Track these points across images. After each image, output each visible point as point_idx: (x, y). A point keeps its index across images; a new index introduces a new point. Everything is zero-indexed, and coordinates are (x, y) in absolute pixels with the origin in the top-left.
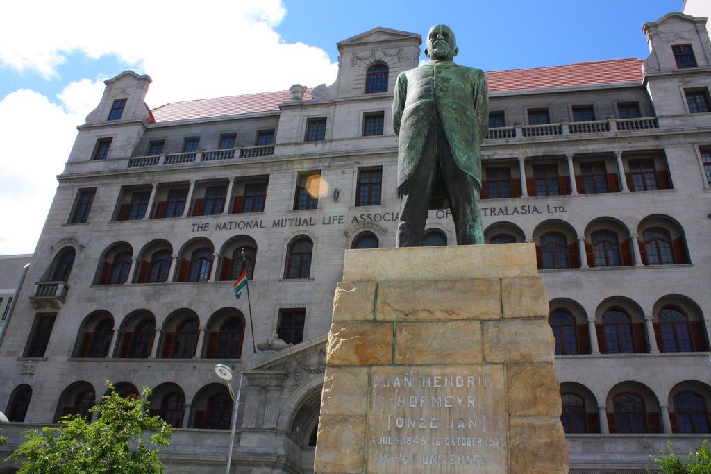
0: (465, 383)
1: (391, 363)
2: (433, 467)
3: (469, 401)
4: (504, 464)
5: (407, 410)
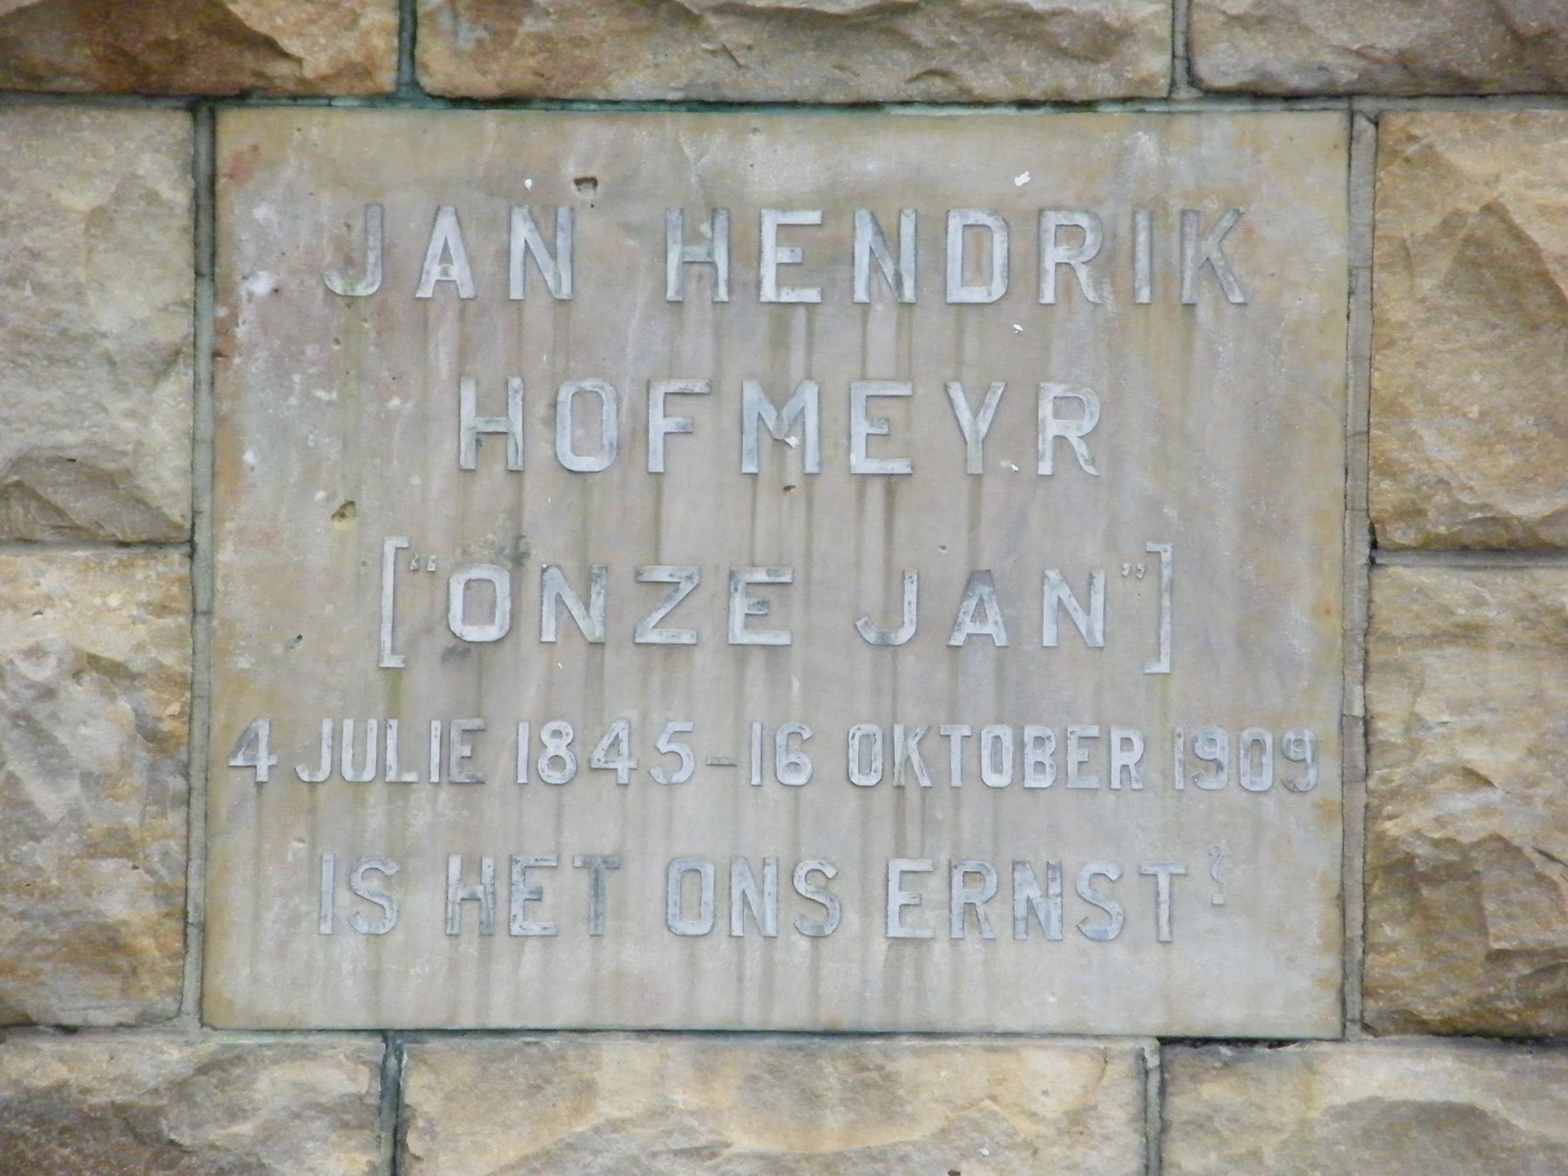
0: (1023, 271)
1: (386, 79)
2: (753, 965)
3: (1052, 428)
4: (1313, 937)
5: (538, 499)
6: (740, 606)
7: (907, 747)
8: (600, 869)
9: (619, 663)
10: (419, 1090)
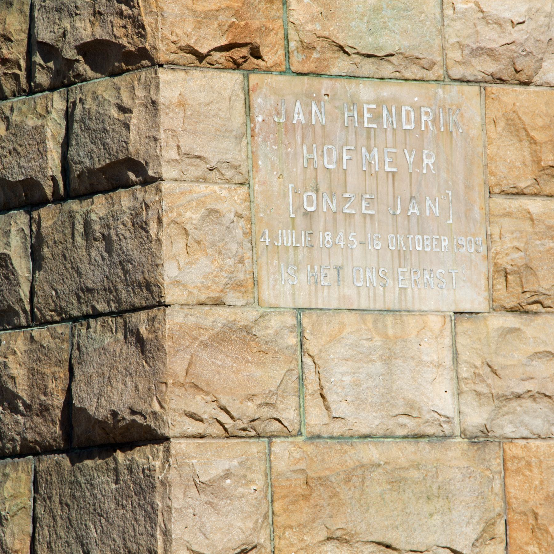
0: (418, 121)
6: (364, 204)
7: (401, 240)
8: (339, 269)
9: (340, 217)
10: (305, 322)
